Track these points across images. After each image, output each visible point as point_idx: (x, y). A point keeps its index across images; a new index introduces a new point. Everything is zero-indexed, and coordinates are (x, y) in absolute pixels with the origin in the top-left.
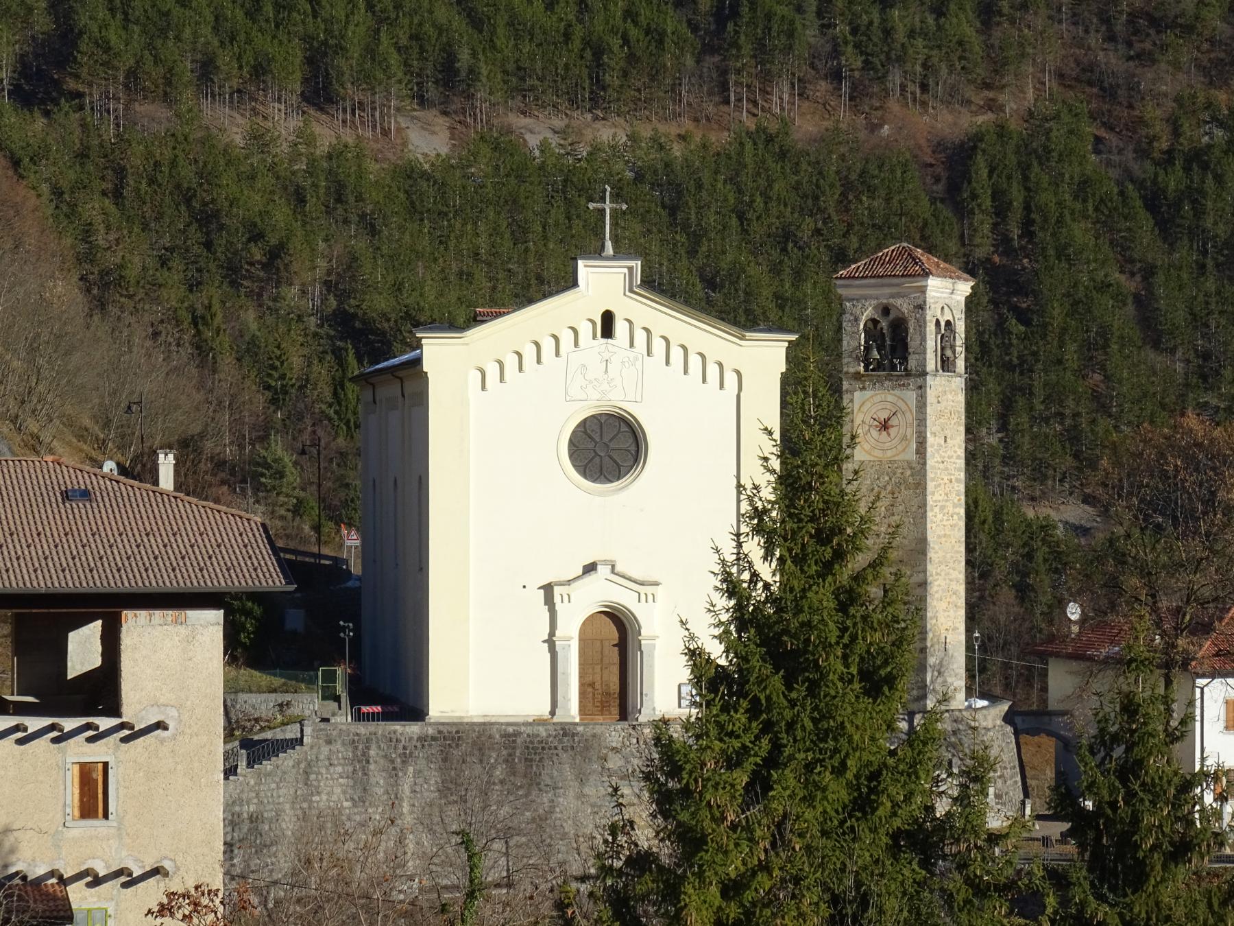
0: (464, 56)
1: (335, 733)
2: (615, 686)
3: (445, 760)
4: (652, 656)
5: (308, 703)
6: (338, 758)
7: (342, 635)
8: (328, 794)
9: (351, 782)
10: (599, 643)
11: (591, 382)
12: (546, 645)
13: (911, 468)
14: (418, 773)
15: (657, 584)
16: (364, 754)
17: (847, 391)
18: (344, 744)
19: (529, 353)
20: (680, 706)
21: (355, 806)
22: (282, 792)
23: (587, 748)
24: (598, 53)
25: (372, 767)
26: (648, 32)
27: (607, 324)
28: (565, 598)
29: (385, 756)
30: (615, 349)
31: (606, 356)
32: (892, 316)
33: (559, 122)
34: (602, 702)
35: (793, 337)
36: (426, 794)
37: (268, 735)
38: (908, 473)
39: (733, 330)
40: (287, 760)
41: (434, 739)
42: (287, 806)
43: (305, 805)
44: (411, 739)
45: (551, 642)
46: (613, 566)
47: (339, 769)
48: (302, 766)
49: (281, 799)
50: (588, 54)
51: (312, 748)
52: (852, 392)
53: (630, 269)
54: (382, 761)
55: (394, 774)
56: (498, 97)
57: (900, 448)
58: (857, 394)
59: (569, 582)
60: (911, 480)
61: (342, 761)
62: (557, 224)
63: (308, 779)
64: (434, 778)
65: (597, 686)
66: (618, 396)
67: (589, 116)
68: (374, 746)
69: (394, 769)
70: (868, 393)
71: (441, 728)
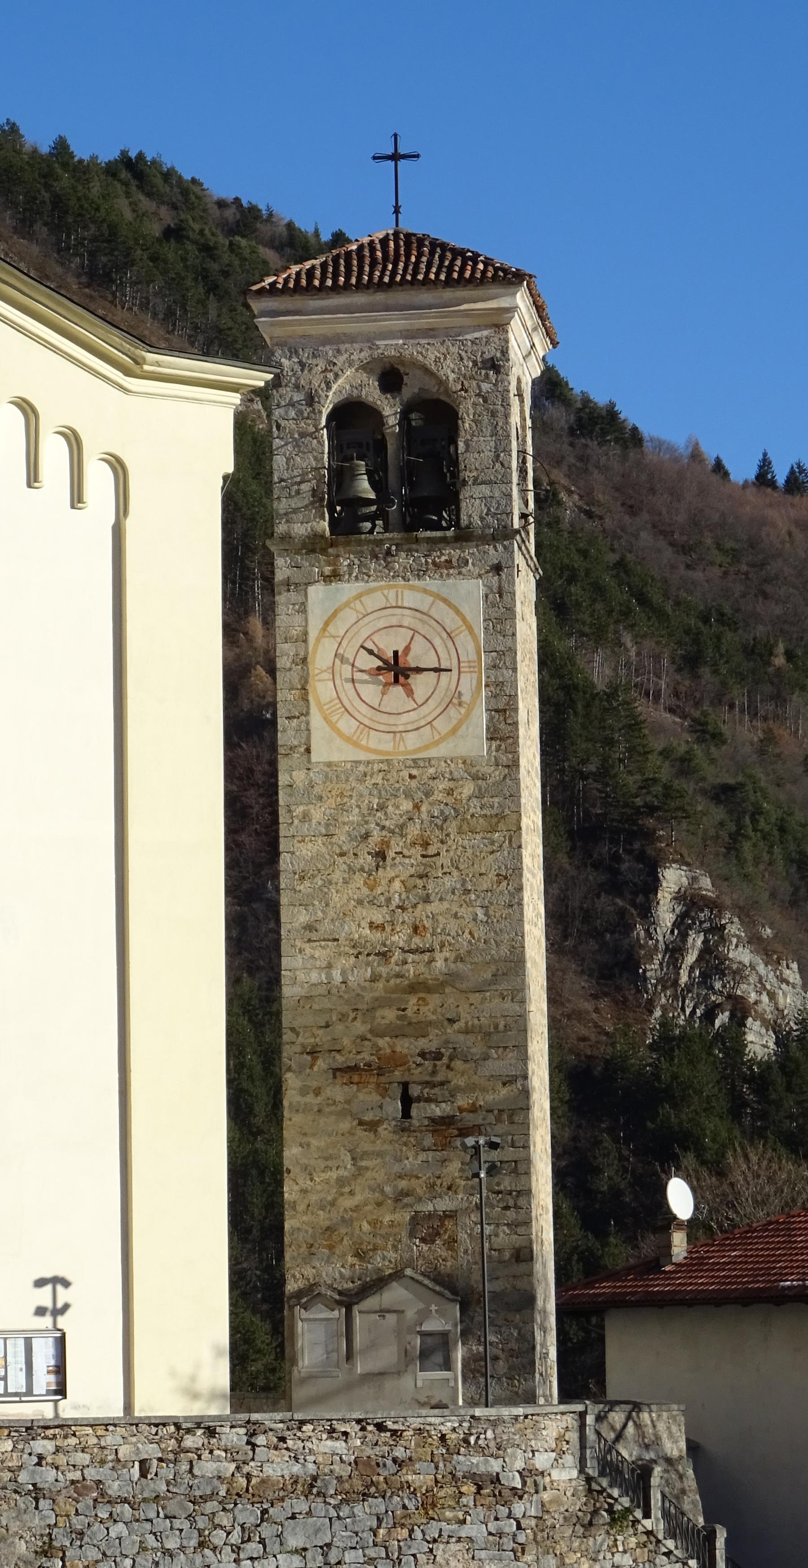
13: (475, 778)
17: (287, 583)
32: (408, 392)
35: (258, 378)
38: (468, 789)
39: (113, 342)
52: (302, 586)
58: (316, 592)
60: (475, 807)
70: (347, 589)
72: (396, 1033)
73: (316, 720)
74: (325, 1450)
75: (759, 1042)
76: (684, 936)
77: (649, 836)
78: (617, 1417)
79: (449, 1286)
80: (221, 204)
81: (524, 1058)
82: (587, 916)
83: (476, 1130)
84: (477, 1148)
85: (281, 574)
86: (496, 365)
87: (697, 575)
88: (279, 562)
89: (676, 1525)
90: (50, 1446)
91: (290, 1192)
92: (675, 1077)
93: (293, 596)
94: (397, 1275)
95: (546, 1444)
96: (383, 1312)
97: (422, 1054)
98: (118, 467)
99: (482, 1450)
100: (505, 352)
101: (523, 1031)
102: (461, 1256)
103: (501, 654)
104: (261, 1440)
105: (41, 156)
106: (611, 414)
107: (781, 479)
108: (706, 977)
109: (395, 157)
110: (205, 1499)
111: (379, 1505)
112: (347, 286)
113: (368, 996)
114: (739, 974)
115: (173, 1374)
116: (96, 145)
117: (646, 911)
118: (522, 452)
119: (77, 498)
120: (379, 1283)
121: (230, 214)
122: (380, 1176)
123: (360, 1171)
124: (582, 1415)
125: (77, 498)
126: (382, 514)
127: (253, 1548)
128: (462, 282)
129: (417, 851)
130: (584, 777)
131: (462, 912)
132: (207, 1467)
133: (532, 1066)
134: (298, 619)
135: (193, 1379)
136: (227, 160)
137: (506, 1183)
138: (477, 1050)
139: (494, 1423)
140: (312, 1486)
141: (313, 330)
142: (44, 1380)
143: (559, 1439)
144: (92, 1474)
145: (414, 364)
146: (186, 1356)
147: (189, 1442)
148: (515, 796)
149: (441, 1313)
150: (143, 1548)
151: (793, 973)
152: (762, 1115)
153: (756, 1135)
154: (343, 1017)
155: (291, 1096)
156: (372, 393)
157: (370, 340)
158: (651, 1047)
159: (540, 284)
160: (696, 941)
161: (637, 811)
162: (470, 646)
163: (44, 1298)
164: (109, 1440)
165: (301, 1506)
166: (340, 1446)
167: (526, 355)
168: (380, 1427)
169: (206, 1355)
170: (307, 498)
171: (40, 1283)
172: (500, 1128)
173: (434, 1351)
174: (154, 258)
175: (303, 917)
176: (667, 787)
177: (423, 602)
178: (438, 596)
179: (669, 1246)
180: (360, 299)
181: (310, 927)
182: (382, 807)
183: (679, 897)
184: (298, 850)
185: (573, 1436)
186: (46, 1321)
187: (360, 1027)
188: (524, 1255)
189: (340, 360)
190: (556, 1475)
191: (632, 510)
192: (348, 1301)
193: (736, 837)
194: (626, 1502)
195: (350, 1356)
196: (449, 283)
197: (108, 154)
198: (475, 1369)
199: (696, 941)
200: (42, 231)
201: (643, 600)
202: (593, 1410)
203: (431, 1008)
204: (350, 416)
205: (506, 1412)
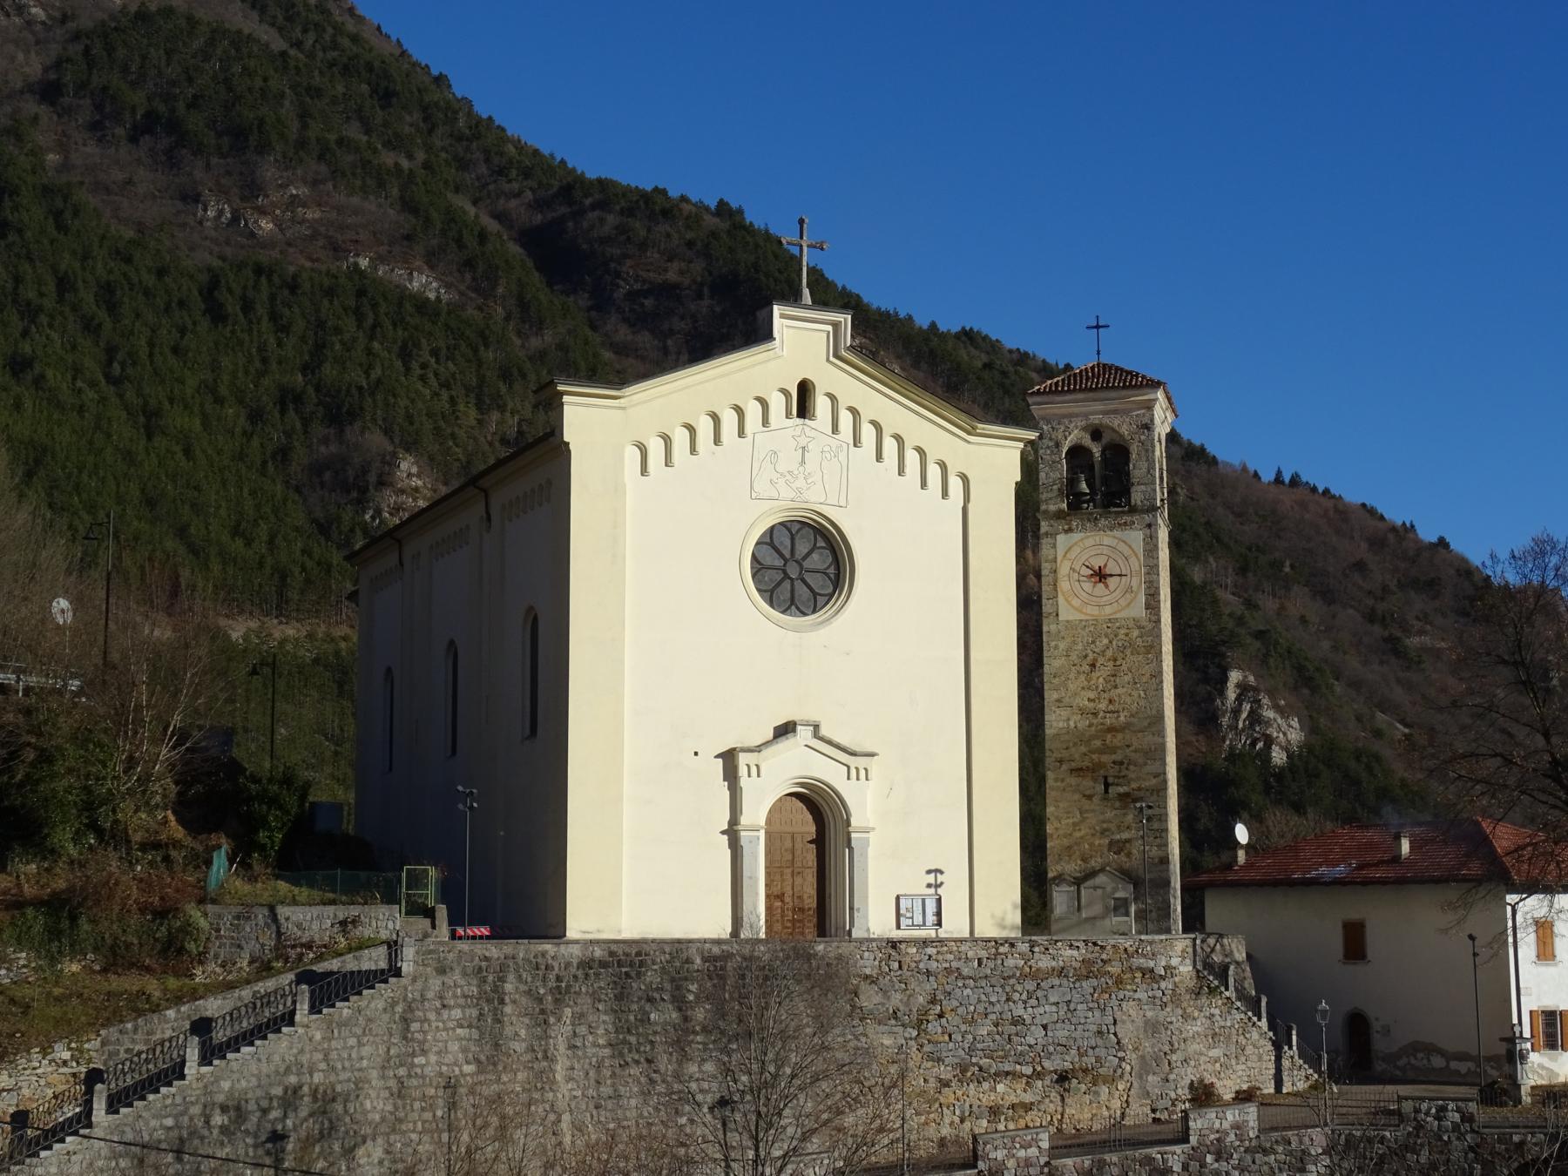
0: (185, 574)
2: (811, 901)
3: (619, 997)
4: (865, 855)
5: (384, 920)
6: (455, 996)
7: (461, 806)
8: (439, 1053)
9: (475, 1034)
14: (579, 1018)
15: (872, 755)
16: (495, 989)
17: (1047, 534)
18: (464, 974)
19: (705, 427)
20: (898, 927)
21: (480, 1071)
22: (366, 1051)
23: (829, 976)
24: (283, 578)
25: (508, 1009)
26: (319, 564)
28: (754, 770)
30: (813, 434)
31: (803, 441)
32: (1104, 441)
33: (254, 624)
36: (590, 1051)
37: (334, 965)
38: (1136, 633)
39: (962, 419)
40: (375, 1001)
41: (603, 964)
42: (374, 1074)
43: (402, 1072)
44: (568, 965)
45: (732, 833)
46: (816, 727)
48: (399, 1009)
49: (365, 1063)
51: (414, 980)
52: (1054, 535)
53: (836, 325)
54: (524, 1000)
55: (542, 1021)
57: (1123, 602)
58: (1061, 538)
59: (758, 749)
61: (461, 1001)
63: (407, 1029)
64: (604, 1022)
65: (787, 899)
66: (819, 494)
68: (511, 977)
69: (543, 1012)
70: (1076, 536)
71: (614, 947)
72: (1101, 751)
73: (1061, 599)
74: (1069, 955)
75: (1278, 757)
77: (1223, 656)
78: (1211, 941)
79: (1127, 875)
80: (1011, 351)
81: (1164, 764)
83: (1141, 799)
86: (1148, 427)
87: (1246, 528)
89: (1241, 994)
90: (934, 951)
91: (1049, 829)
94: (1102, 870)
95: (1176, 954)
96: (1095, 888)
98: (964, 478)
99: (1144, 956)
100: (1152, 420)
102: (1134, 861)
104: (1036, 949)
105: (1417, 541)
106: (1202, 449)
107: (1287, 480)
108: (1252, 726)
109: (1098, 327)
111: (1094, 982)
114: (1268, 723)
115: (993, 916)
117: (1222, 692)
119: (945, 494)
120: (1093, 874)
121: (1015, 356)
123: (1084, 820)
125: (945, 494)
126: (1092, 500)
127: (1033, 1002)
129: (1111, 663)
132: (1010, 962)
136: (1014, 330)
137: (1156, 825)
138: (1141, 761)
139: (1151, 943)
140: (1061, 972)
142: (931, 919)
144: (954, 964)
146: (998, 905)
147: (1002, 950)
148: (1159, 636)
149: (1124, 889)
150: (979, 1001)
151: (1295, 723)
154: (1075, 744)
155: (1050, 782)
156: (1087, 441)
157: (1086, 415)
158: (1225, 759)
159: (1168, 387)
160: (1247, 707)
162: (1137, 564)
163: (931, 879)
164: (963, 948)
165: (1056, 982)
166: (1075, 953)
169: (1009, 907)
170: (1056, 493)
171: (929, 872)
173: (1121, 907)
175: (1055, 696)
177: (1114, 542)
180: (1080, 396)
181: (1059, 701)
183: (1238, 685)
184: (1053, 663)
185: (1190, 950)
186: (932, 891)
187: (1083, 749)
188: (1165, 861)
191: (1213, 496)
192: (1078, 882)
193: (1267, 655)
196: (1124, 387)
197: (956, 329)
198: (1141, 916)
199: (1247, 707)
200: (924, 366)
201: (1218, 540)
203: (1118, 740)
204: (1076, 452)
205: (1157, 937)
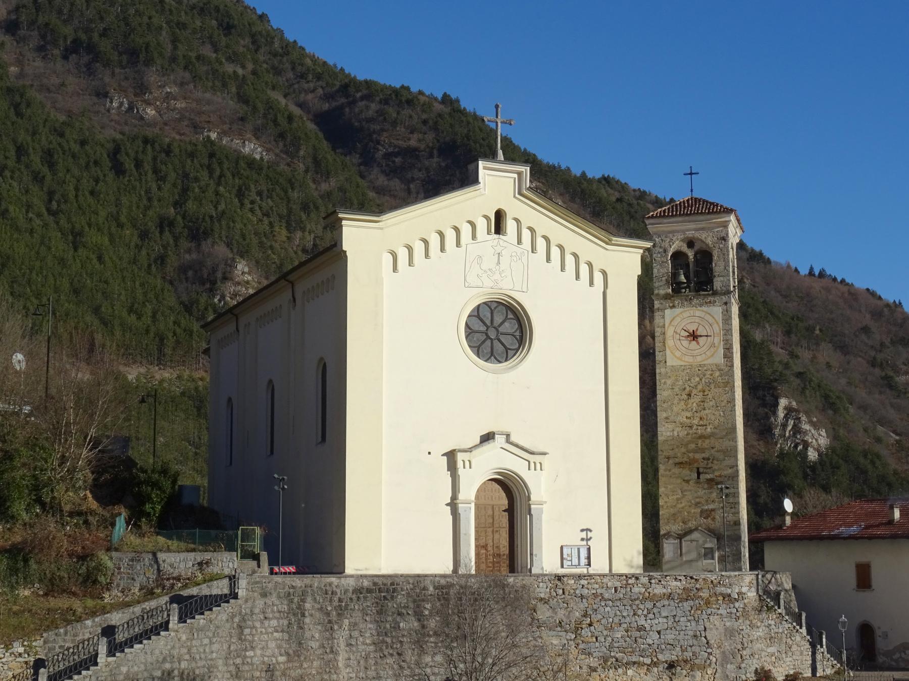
1: (270, 585)
2: (505, 550)
4: (540, 519)
5: (226, 562)
6: (273, 611)
7: (276, 488)
8: (263, 649)
9: (286, 636)
10: (490, 508)
11: (485, 271)
12: (449, 508)
13: (719, 370)
14: (353, 625)
15: (545, 454)
16: (299, 607)
17: (658, 309)
18: (279, 597)
19: (434, 240)
20: (562, 567)
22: (215, 647)
23: (517, 599)
24: (162, 340)
25: (307, 620)
26: (185, 330)
27: (499, 222)
29: (321, 609)
30: (505, 244)
31: (499, 249)
32: (697, 247)
33: (143, 370)
34: (493, 563)
35: (648, 245)
36: (361, 647)
37: (194, 591)
38: (717, 374)
40: (220, 614)
41: (369, 591)
42: (220, 662)
43: (238, 661)
44: (346, 591)
45: (453, 505)
46: (508, 436)
47: (274, 623)
48: (236, 620)
50: (157, 339)
51: (246, 601)
53: (520, 174)
54: (318, 615)
55: (329, 627)
56: (113, 357)
58: (668, 312)
59: (470, 450)
60: (720, 379)
61: (277, 615)
62: (144, 413)
63: (242, 633)
64: (370, 628)
66: (510, 286)
67: (157, 368)
68: (309, 599)
69: (330, 622)
70: (677, 311)
71: (376, 580)
72: (695, 451)
73: (668, 352)
74: (675, 585)
76: (787, 421)
77: (775, 389)
78: (769, 576)
80: (634, 190)
82: (755, 415)
83: (721, 483)
84: (722, 489)
85: (656, 307)
86: (724, 239)
87: (790, 305)
88: (656, 302)
89: (789, 612)
90: (586, 582)
91: (661, 502)
92: (785, 466)
93: (660, 313)
94: (696, 529)
95: (746, 583)
96: (692, 541)
97: (704, 459)
98: (604, 273)
100: (727, 235)
101: (736, 451)
102: (717, 523)
103: (727, 331)
104: (653, 581)
106: (761, 254)
107: (817, 273)
108: (795, 435)
109: (691, 174)
110: (635, 600)
111: (691, 603)
112: (676, 215)
113: (686, 440)
114: (805, 433)
115: (625, 560)
116: (594, 173)
117: (775, 413)
118: (733, 266)
119: (591, 283)
120: (690, 532)
121: (637, 193)
122: (690, 497)
123: (684, 496)
124: (757, 575)
125: (591, 283)
126: (688, 287)
127: (651, 616)
128: (713, 213)
130: (753, 370)
131: (716, 413)
132: (636, 590)
133: (739, 463)
134: (662, 320)
135: (631, 561)
137: (731, 500)
138: (721, 457)
139: (729, 577)
140: (670, 596)
141: (665, 229)
142: (584, 561)
143: (750, 583)
144: (599, 591)
145: (698, 239)
146: (629, 553)
147: (630, 581)
148: (732, 376)
150: (616, 615)
151: (823, 433)
152: (814, 479)
153: (812, 485)
154: (678, 447)
156: (685, 248)
157: (684, 232)
158: (777, 457)
159: (738, 212)
160: (791, 422)
161: (771, 381)
162: (718, 328)
163: (584, 535)
164: (605, 580)
165: (666, 603)
166: (678, 583)
167: (734, 235)
168: (692, 578)
169: (635, 554)
171: (582, 530)
172: (730, 482)
173: (709, 554)
174: (613, 208)
175: (665, 415)
176: (781, 373)
178: (706, 312)
179: (785, 521)
180: (680, 219)
181: (667, 418)
182: (689, 380)
183: (785, 408)
184: (663, 393)
185: (755, 582)
186: (584, 543)
187: (683, 450)
188: (737, 523)
189: (674, 239)
190: (749, 594)
191: (768, 284)
192: (680, 537)
193: (804, 389)
194: (772, 603)
195: (681, 555)
197: (598, 176)
198: (722, 560)
199: (791, 422)
200: (578, 200)
201: (772, 313)
202: (761, 574)
203: (706, 444)
204: (678, 256)
205: (733, 574)
